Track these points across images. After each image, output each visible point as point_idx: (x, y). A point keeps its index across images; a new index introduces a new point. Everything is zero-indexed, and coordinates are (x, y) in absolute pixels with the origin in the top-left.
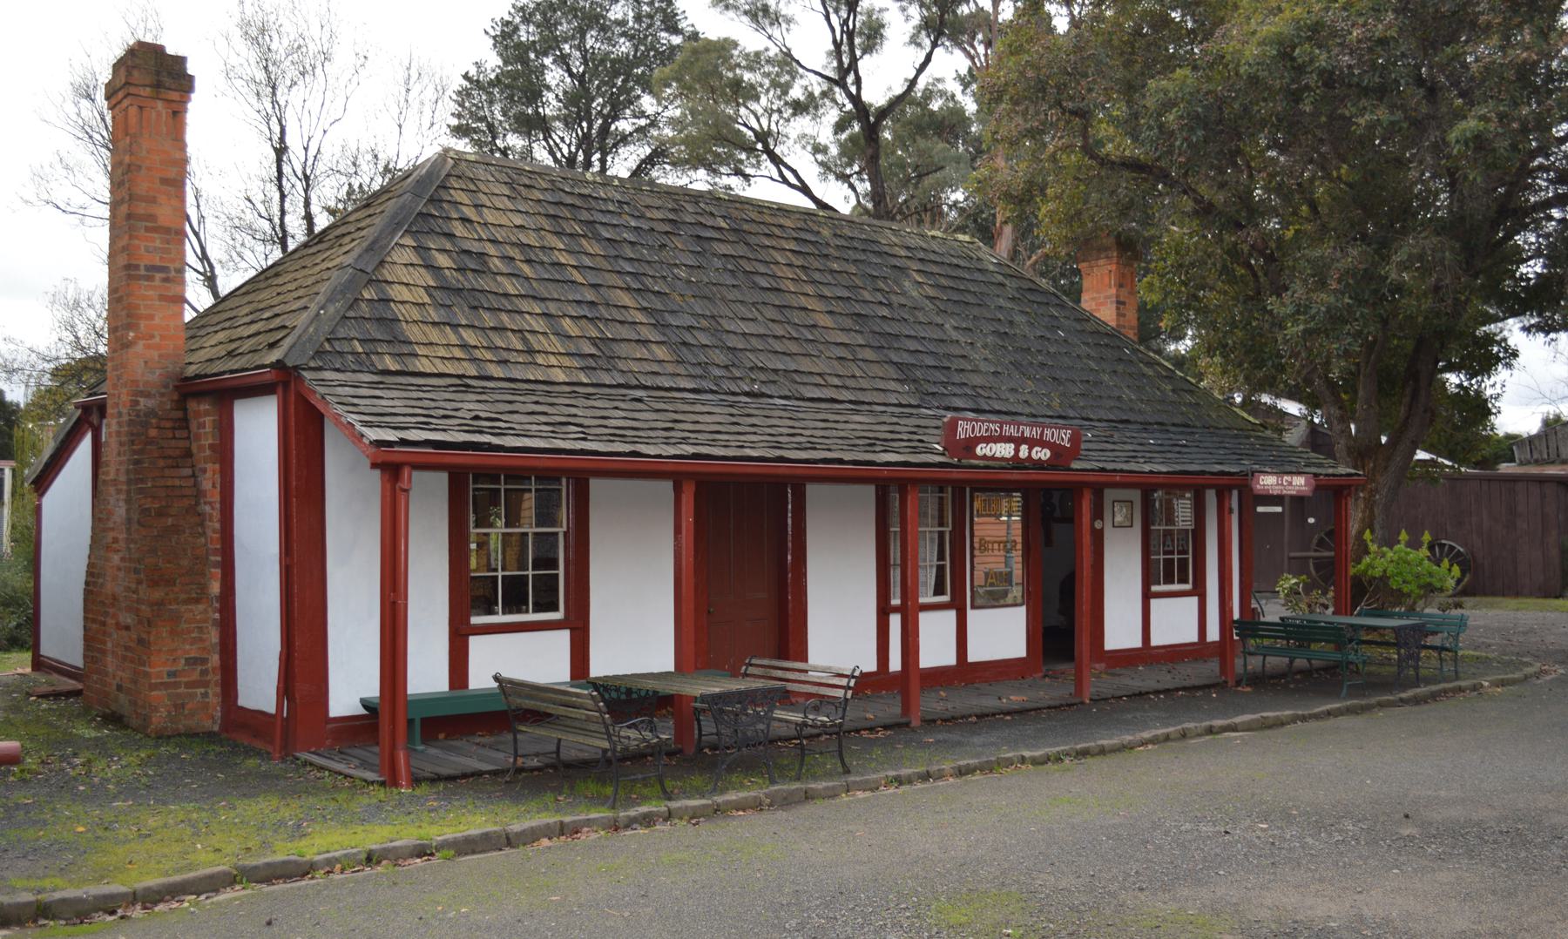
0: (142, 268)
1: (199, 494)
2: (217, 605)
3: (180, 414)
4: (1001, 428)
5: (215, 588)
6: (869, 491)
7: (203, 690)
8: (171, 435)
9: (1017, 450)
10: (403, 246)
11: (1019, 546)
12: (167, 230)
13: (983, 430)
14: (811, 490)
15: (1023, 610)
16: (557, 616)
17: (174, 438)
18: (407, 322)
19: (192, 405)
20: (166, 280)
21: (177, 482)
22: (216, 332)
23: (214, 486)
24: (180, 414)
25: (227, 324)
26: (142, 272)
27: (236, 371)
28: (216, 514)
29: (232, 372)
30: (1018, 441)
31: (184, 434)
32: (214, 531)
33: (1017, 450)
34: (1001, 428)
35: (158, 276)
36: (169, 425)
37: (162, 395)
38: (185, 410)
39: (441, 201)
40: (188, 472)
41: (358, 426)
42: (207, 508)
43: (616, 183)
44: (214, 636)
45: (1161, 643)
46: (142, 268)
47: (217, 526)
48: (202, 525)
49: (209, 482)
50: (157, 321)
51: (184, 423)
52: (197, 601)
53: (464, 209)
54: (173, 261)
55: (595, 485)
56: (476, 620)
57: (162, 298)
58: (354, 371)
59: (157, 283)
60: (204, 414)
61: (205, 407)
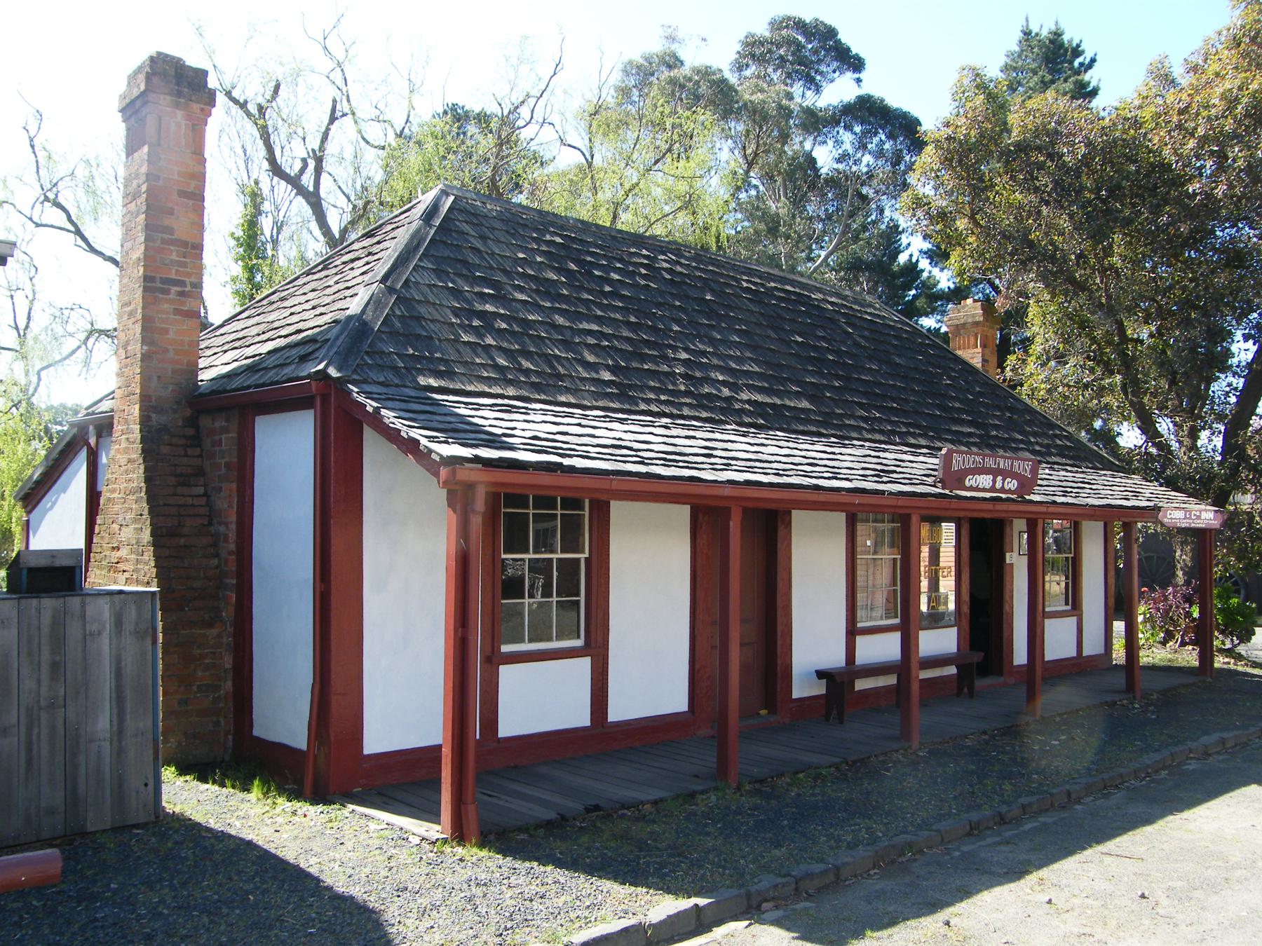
0: (158, 280)
1: (212, 515)
2: (231, 630)
3: (190, 432)
4: (983, 460)
5: (228, 613)
6: (841, 518)
7: (215, 719)
8: (183, 453)
9: (994, 481)
10: (423, 267)
11: (953, 573)
12: (185, 244)
13: (971, 462)
14: (618, 509)
15: (955, 629)
16: (579, 643)
17: (186, 455)
18: (440, 340)
19: (205, 422)
20: (182, 294)
21: (189, 500)
22: (225, 352)
23: (230, 506)
24: (190, 432)
25: (237, 344)
26: (158, 285)
27: (264, 385)
28: (232, 536)
29: (257, 386)
30: (995, 472)
31: (197, 451)
32: (230, 553)
33: (994, 481)
34: (983, 460)
35: (175, 289)
36: (182, 442)
37: (175, 411)
38: (198, 428)
39: (450, 230)
40: (201, 490)
41: (424, 441)
42: (222, 529)
43: (593, 229)
44: (228, 661)
45: (1051, 659)
46: (158, 280)
47: (232, 547)
48: (215, 545)
49: (226, 504)
50: (171, 335)
51: (196, 440)
52: (211, 625)
53: (472, 240)
54: (189, 275)
55: (617, 508)
56: (505, 648)
57: (178, 312)
58: (397, 386)
59: (172, 296)
60: (222, 431)
61: (220, 423)
